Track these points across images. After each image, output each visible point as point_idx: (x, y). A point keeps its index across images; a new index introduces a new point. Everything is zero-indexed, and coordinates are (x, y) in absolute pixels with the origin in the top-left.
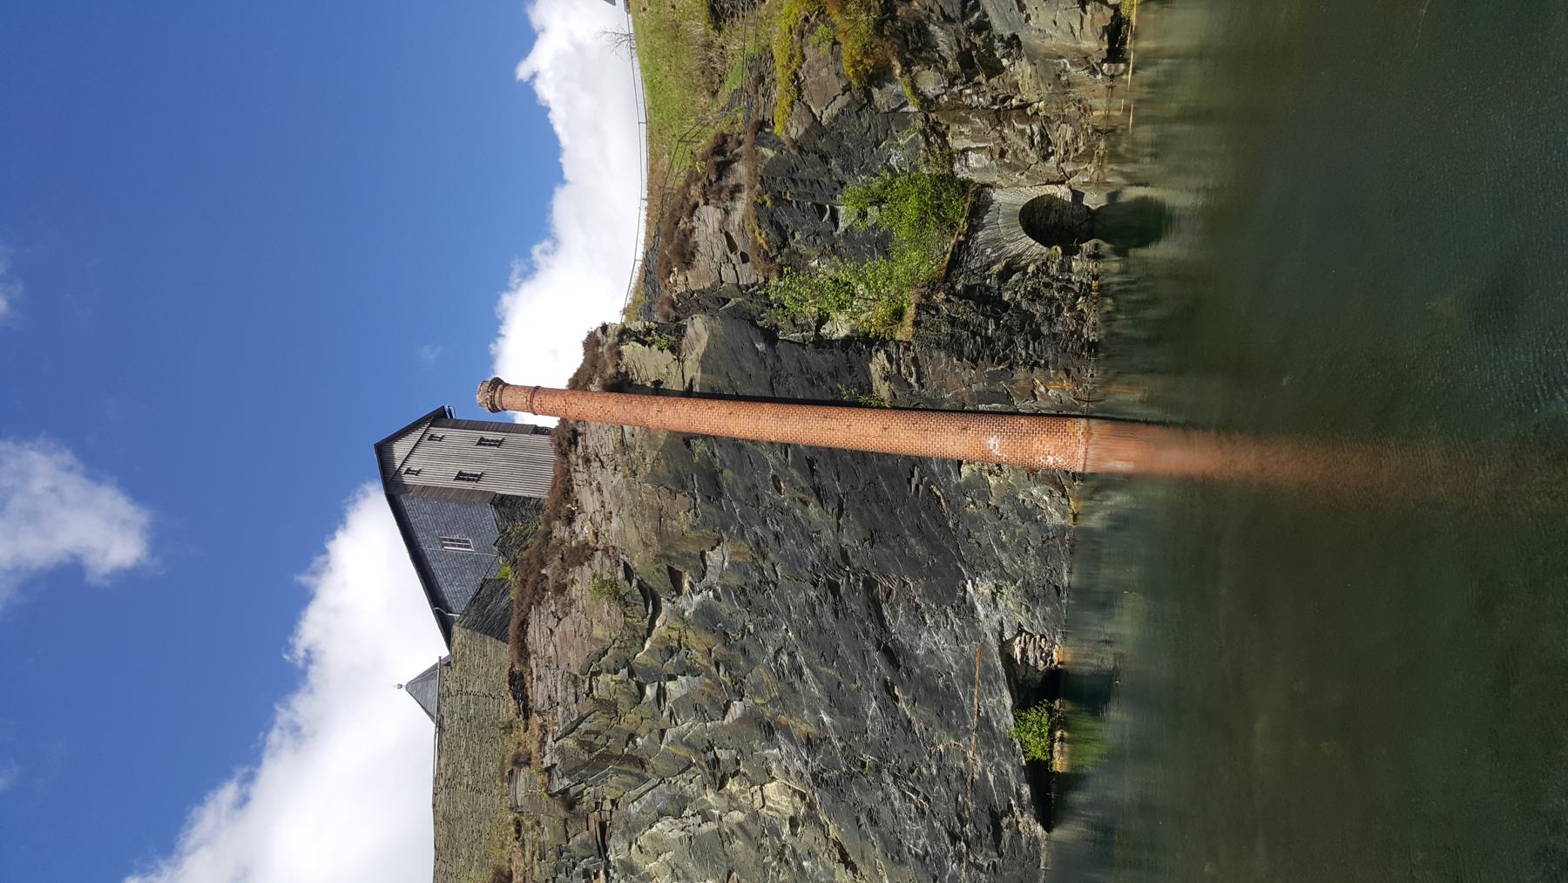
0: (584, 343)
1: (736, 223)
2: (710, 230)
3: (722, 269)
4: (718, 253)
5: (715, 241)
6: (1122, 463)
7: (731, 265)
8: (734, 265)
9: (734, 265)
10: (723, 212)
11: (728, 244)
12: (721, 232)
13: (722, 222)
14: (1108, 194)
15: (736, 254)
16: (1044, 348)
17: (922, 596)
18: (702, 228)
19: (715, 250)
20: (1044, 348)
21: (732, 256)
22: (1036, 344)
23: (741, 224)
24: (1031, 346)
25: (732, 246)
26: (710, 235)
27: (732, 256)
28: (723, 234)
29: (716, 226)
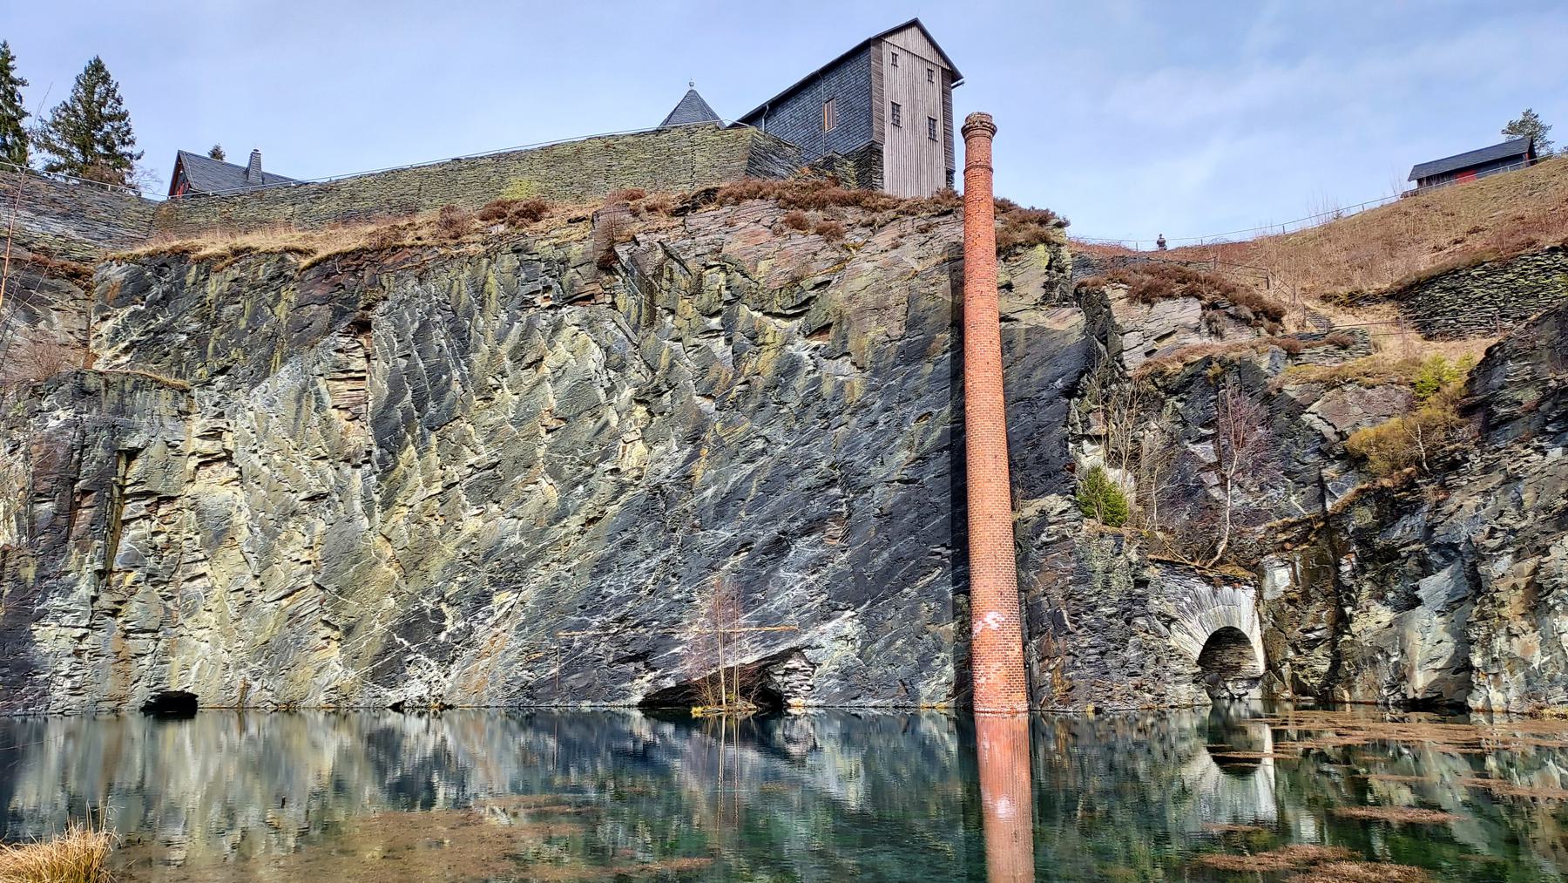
29: (1182, 321)
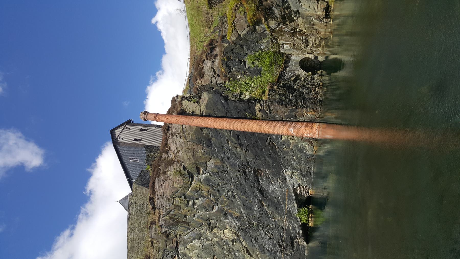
0: (171, 101)
1: (216, 65)
2: (208, 68)
3: (212, 79)
4: (211, 74)
5: (210, 71)
6: (329, 136)
7: (214, 78)
8: (215, 78)
9: (215, 78)
10: (212, 62)
11: (214, 72)
12: (212, 68)
13: (212, 65)
14: (325, 57)
15: (216, 74)
16: (306, 102)
17: (270, 175)
18: (206, 67)
19: (210, 73)
20: (306, 102)
21: (215, 75)
22: (304, 101)
23: (217, 66)
24: (302, 101)
25: (215, 72)
26: (208, 69)
27: (215, 75)
28: (212, 69)
29: (210, 66)
